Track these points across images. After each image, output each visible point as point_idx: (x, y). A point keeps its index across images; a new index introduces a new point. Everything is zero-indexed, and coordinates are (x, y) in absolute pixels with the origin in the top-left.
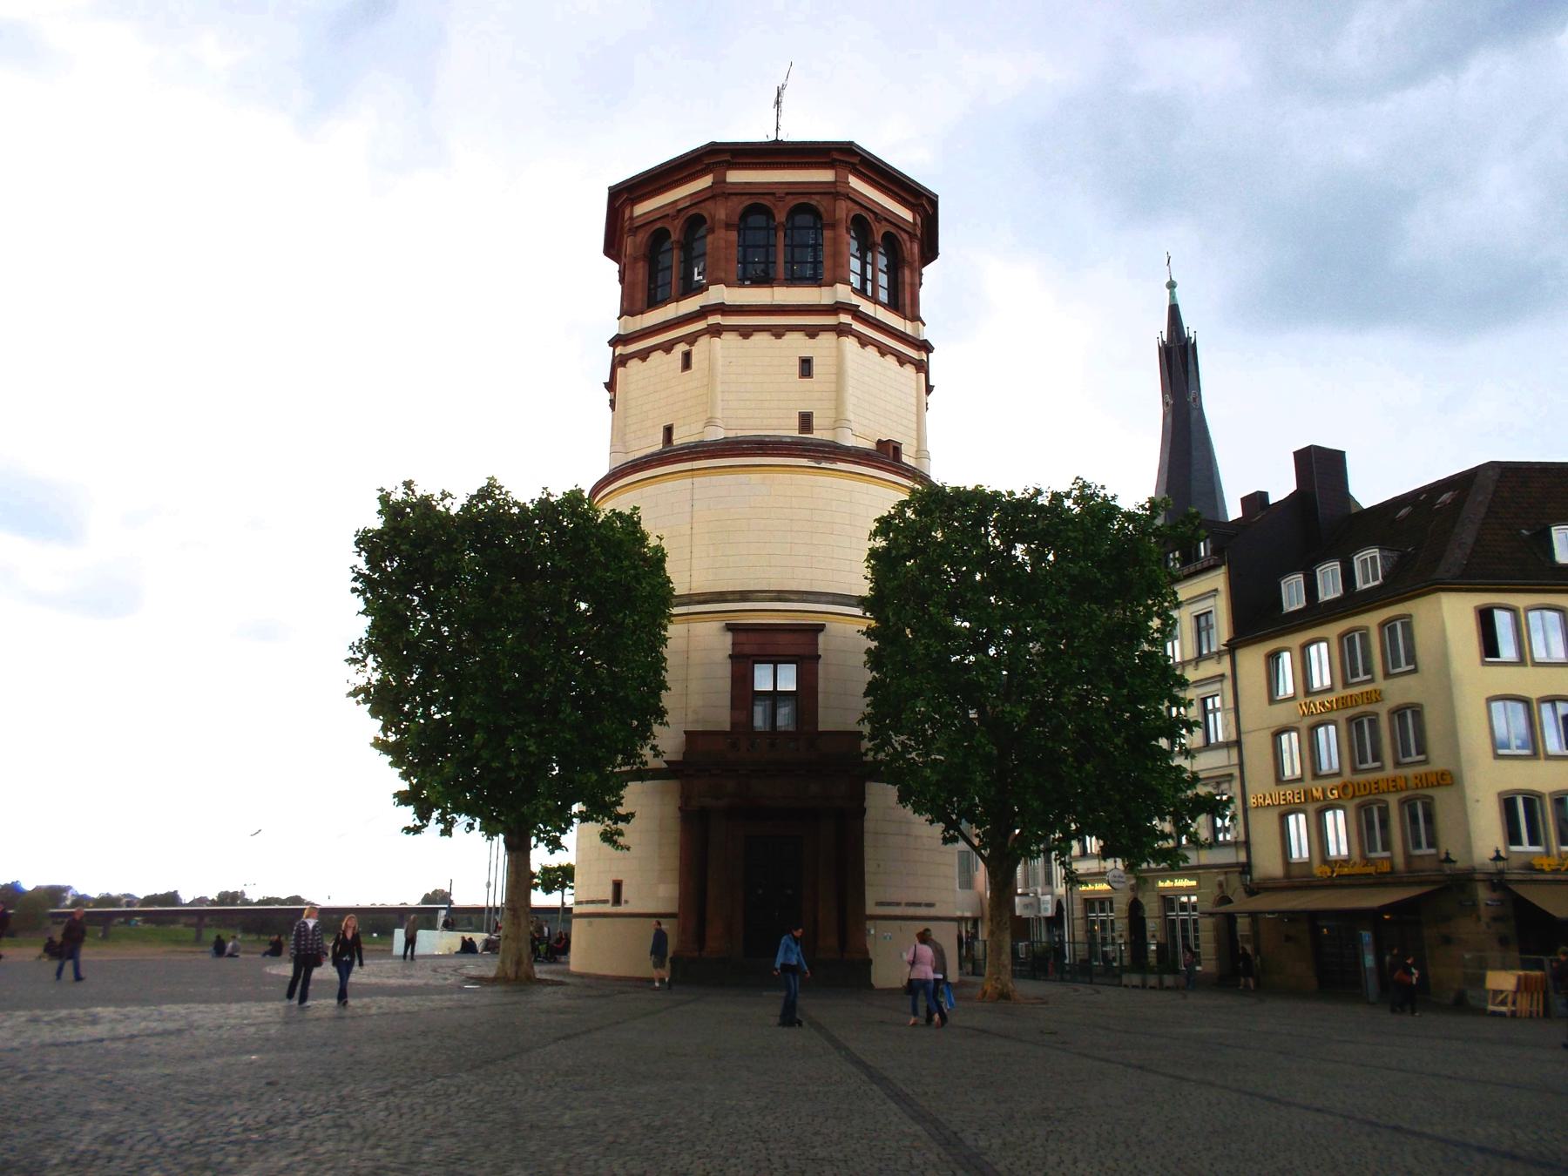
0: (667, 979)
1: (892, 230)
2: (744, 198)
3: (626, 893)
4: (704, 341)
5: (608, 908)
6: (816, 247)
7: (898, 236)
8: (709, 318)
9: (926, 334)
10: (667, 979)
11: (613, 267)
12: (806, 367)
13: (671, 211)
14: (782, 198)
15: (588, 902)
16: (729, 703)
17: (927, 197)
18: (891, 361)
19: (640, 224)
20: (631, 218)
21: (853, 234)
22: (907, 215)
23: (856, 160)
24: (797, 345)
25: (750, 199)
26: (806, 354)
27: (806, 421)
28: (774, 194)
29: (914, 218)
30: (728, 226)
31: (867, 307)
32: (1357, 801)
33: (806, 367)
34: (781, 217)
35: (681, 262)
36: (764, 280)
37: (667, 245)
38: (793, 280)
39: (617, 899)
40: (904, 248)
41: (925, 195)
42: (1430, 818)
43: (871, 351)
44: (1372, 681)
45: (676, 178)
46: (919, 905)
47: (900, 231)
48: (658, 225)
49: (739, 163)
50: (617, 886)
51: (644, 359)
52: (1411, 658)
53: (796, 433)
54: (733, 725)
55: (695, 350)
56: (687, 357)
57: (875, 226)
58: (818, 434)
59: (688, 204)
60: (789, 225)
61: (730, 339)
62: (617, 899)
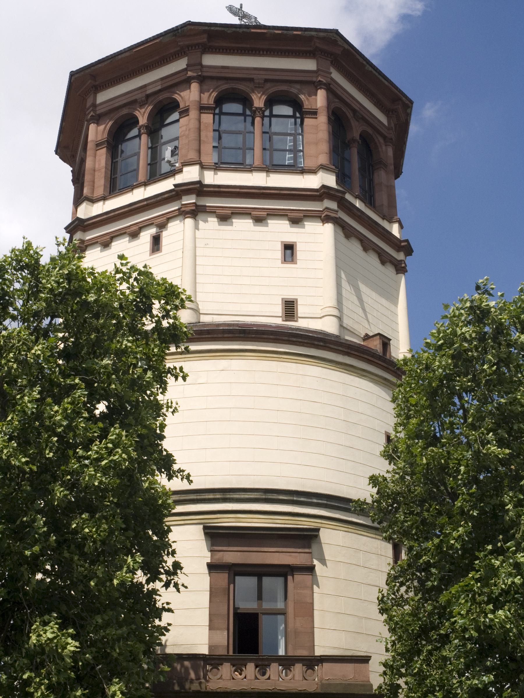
0: (477, 596)
1: (370, 131)
3: (301, 310)
8: (183, 197)
10: (477, 596)
13: (139, 96)
16: (207, 624)
18: (373, 260)
19: (103, 111)
20: (94, 105)
25: (226, 83)
26: (157, 255)
30: (203, 109)
35: (149, 148)
40: (380, 150)
48: (125, 111)
53: (279, 321)
55: (165, 235)
56: (156, 241)
57: (354, 123)
58: (302, 324)
59: (159, 88)
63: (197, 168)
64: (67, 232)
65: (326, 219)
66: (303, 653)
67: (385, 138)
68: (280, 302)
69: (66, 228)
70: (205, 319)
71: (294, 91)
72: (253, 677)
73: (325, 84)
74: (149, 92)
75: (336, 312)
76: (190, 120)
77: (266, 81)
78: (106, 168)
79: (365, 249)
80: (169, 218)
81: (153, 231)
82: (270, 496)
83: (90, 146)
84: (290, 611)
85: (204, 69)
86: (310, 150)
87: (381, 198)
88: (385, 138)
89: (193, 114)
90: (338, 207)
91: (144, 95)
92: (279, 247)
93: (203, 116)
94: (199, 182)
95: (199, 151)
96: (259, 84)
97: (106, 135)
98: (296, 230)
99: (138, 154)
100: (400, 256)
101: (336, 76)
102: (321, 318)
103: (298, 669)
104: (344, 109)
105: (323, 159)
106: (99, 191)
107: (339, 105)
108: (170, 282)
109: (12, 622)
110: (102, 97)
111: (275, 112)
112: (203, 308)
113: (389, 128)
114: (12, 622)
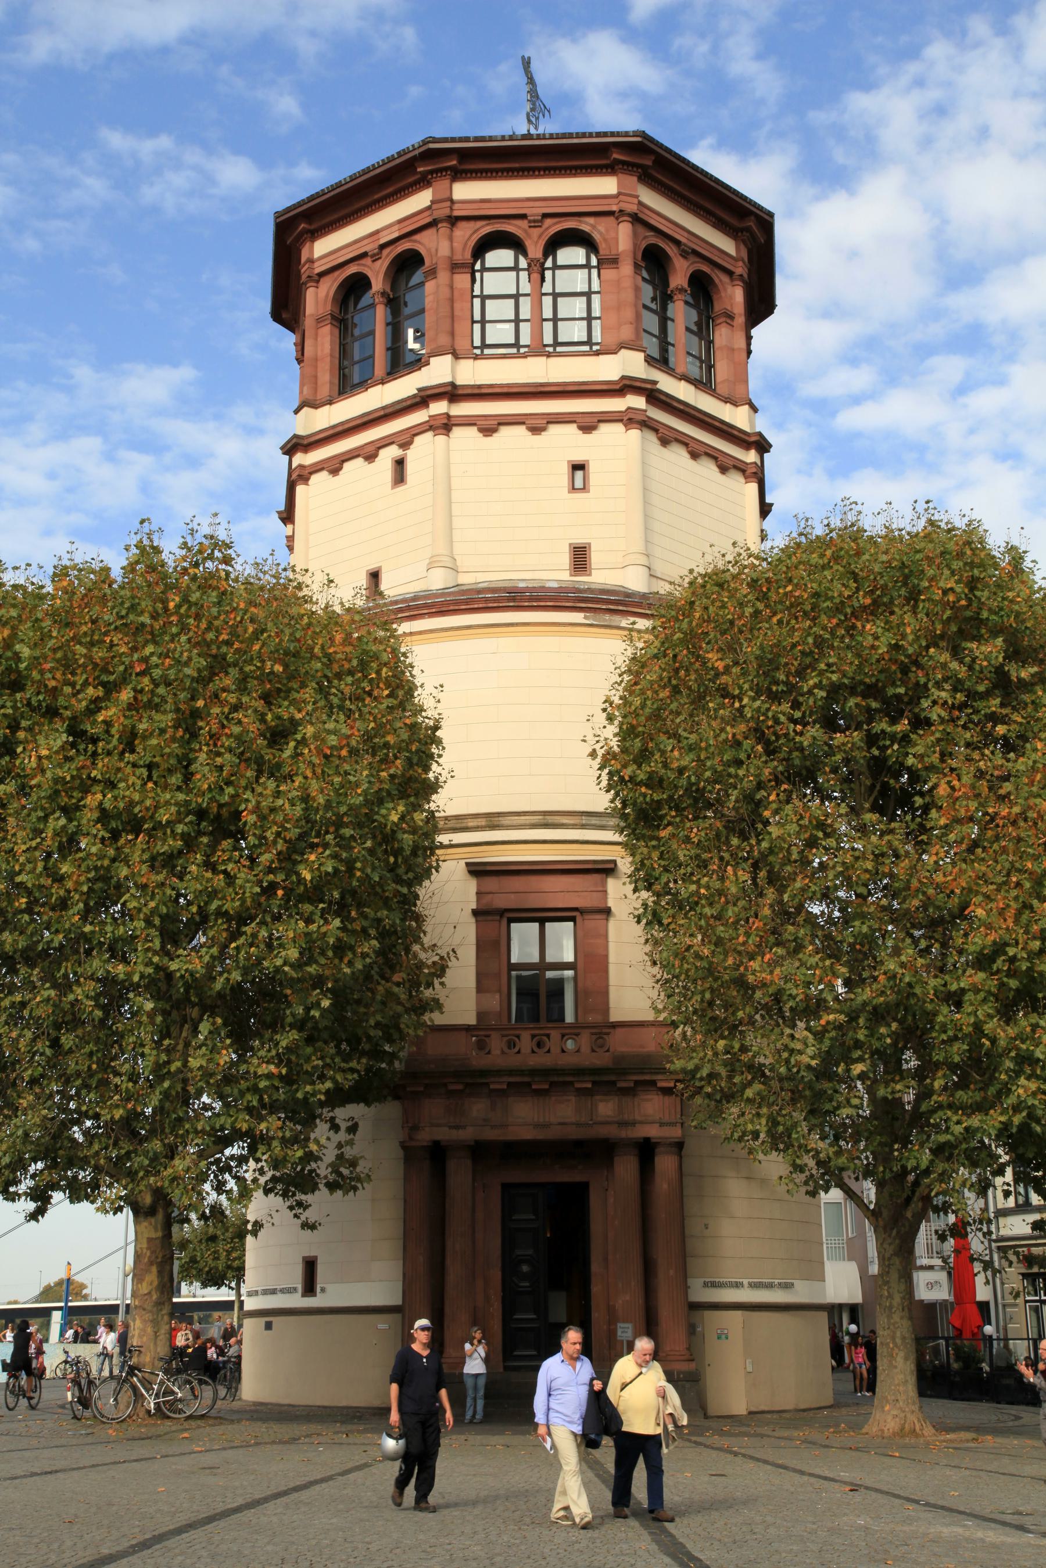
1: (705, 268)
2: (336, 273)
3: (596, 558)
7: (717, 281)
9: (762, 425)
13: (370, 247)
14: (688, 253)
17: (757, 216)
18: (708, 469)
20: (311, 261)
21: (645, 274)
22: (726, 244)
26: (401, 488)
27: (580, 557)
28: (523, 217)
29: (738, 249)
31: (668, 385)
41: (751, 213)
45: (376, 197)
46: (770, 1286)
47: (417, 237)
48: (352, 269)
49: (471, 171)
51: (335, 471)
59: (396, 235)
64: (285, 453)
68: (567, 549)
69: (282, 448)
72: (529, 1050)
73: (629, 215)
74: (382, 241)
75: (643, 560)
76: (438, 286)
77: (546, 216)
78: (332, 356)
79: (694, 456)
85: (456, 206)
87: (722, 370)
89: (443, 276)
90: (648, 402)
91: (376, 245)
92: (565, 469)
93: (457, 277)
95: (452, 334)
96: (535, 221)
97: (329, 307)
99: (372, 333)
100: (751, 457)
104: (662, 244)
107: (653, 239)
112: (462, 563)
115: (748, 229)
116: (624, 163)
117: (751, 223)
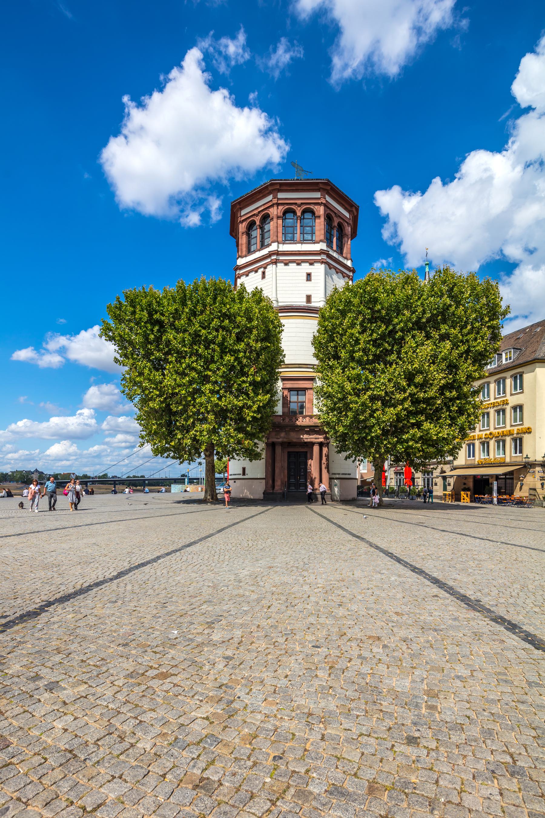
1: (342, 221)
4: (270, 268)
5: (241, 477)
6: (312, 227)
11: (319, 249)
12: (309, 275)
15: (234, 475)
22: (347, 215)
23: (329, 188)
24: (306, 268)
26: (309, 271)
27: (309, 298)
30: (278, 217)
31: (331, 252)
32: (495, 409)
33: (309, 275)
34: (299, 214)
36: (293, 241)
37: (255, 228)
38: (303, 241)
39: (244, 474)
42: (521, 445)
43: (293, 266)
44: (505, 396)
46: (346, 474)
50: (244, 469)
51: (247, 275)
52: (521, 387)
53: (305, 304)
54: (283, 413)
56: (264, 273)
57: (335, 219)
58: (313, 304)
60: (302, 217)
61: (280, 266)
62: (244, 474)
63: (276, 243)
65: (322, 263)
66: (310, 414)
67: (347, 223)
70: (280, 304)
71: (312, 207)
80: (268, 264)
81: (262, 270)
82: (300, 366)
83: (240, 234)
84: (307, 401)
86: (317, 233)
88: (347, 223)
92: (305, 275)
94: (277, 250)
95: (277, 236)
98: (312, 267)
99: (256, 237)
101: (328, 199)
102: (49, 604)
103: (308, 418)
105: (322, 237)
106: (244, 253)
107: (329, 211)
108: (278, 264)
109: (86, 176)
110: (243, 212)
111: (306, 217)
113: (350, 219)
114: (86, 176)
115: (321, 188)
116: (323, 189)
117: (354, 210)
